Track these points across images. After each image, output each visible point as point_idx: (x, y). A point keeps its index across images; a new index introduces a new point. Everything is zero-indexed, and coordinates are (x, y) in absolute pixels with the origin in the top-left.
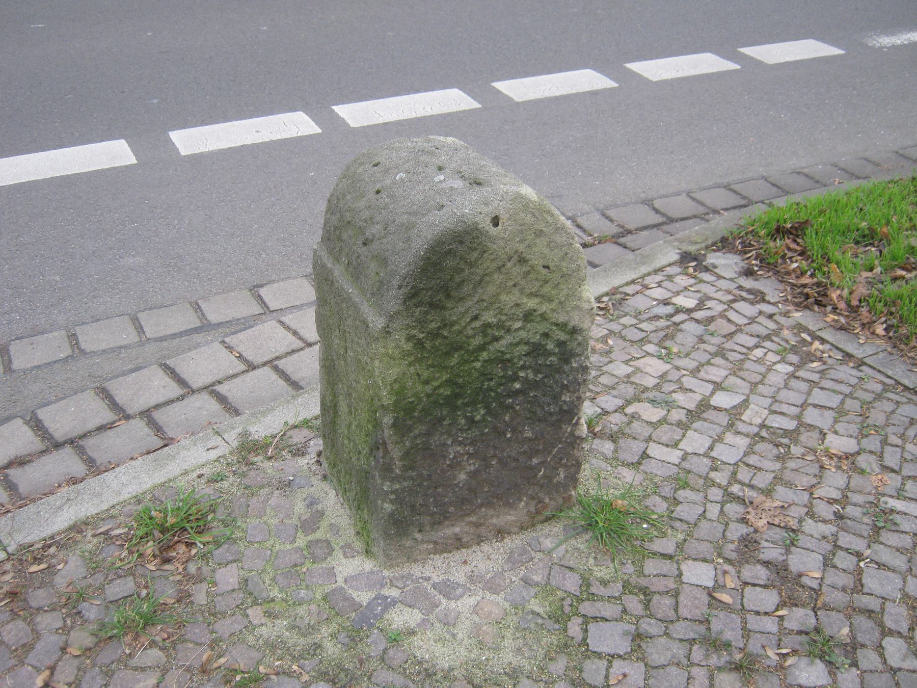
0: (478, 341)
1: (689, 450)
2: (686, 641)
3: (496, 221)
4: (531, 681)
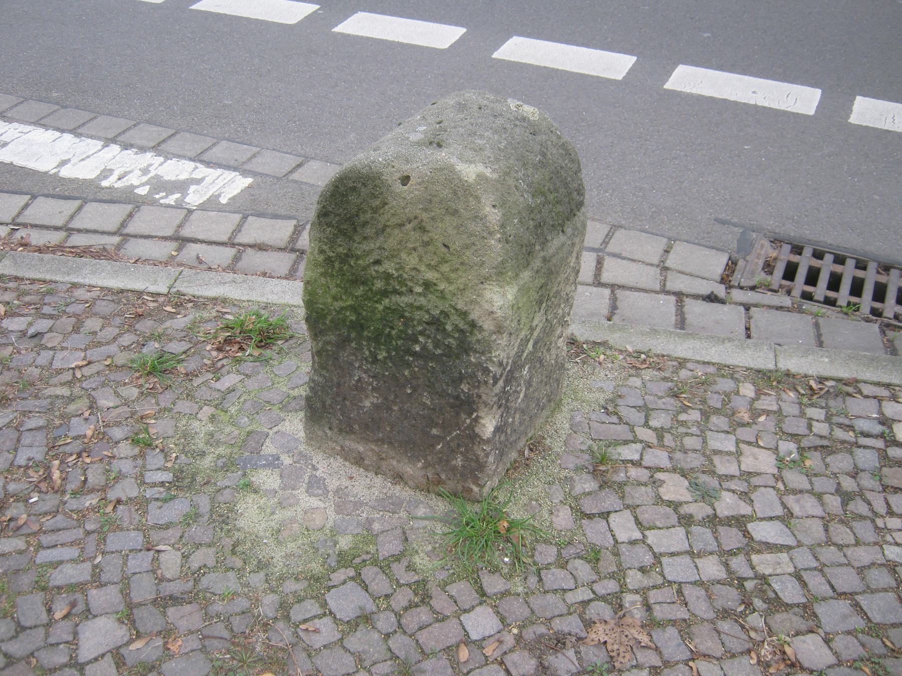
0: (379, 285)
1: (649, 541)
2: (392, 652)
3: (405, 180)
4: (265, 578)
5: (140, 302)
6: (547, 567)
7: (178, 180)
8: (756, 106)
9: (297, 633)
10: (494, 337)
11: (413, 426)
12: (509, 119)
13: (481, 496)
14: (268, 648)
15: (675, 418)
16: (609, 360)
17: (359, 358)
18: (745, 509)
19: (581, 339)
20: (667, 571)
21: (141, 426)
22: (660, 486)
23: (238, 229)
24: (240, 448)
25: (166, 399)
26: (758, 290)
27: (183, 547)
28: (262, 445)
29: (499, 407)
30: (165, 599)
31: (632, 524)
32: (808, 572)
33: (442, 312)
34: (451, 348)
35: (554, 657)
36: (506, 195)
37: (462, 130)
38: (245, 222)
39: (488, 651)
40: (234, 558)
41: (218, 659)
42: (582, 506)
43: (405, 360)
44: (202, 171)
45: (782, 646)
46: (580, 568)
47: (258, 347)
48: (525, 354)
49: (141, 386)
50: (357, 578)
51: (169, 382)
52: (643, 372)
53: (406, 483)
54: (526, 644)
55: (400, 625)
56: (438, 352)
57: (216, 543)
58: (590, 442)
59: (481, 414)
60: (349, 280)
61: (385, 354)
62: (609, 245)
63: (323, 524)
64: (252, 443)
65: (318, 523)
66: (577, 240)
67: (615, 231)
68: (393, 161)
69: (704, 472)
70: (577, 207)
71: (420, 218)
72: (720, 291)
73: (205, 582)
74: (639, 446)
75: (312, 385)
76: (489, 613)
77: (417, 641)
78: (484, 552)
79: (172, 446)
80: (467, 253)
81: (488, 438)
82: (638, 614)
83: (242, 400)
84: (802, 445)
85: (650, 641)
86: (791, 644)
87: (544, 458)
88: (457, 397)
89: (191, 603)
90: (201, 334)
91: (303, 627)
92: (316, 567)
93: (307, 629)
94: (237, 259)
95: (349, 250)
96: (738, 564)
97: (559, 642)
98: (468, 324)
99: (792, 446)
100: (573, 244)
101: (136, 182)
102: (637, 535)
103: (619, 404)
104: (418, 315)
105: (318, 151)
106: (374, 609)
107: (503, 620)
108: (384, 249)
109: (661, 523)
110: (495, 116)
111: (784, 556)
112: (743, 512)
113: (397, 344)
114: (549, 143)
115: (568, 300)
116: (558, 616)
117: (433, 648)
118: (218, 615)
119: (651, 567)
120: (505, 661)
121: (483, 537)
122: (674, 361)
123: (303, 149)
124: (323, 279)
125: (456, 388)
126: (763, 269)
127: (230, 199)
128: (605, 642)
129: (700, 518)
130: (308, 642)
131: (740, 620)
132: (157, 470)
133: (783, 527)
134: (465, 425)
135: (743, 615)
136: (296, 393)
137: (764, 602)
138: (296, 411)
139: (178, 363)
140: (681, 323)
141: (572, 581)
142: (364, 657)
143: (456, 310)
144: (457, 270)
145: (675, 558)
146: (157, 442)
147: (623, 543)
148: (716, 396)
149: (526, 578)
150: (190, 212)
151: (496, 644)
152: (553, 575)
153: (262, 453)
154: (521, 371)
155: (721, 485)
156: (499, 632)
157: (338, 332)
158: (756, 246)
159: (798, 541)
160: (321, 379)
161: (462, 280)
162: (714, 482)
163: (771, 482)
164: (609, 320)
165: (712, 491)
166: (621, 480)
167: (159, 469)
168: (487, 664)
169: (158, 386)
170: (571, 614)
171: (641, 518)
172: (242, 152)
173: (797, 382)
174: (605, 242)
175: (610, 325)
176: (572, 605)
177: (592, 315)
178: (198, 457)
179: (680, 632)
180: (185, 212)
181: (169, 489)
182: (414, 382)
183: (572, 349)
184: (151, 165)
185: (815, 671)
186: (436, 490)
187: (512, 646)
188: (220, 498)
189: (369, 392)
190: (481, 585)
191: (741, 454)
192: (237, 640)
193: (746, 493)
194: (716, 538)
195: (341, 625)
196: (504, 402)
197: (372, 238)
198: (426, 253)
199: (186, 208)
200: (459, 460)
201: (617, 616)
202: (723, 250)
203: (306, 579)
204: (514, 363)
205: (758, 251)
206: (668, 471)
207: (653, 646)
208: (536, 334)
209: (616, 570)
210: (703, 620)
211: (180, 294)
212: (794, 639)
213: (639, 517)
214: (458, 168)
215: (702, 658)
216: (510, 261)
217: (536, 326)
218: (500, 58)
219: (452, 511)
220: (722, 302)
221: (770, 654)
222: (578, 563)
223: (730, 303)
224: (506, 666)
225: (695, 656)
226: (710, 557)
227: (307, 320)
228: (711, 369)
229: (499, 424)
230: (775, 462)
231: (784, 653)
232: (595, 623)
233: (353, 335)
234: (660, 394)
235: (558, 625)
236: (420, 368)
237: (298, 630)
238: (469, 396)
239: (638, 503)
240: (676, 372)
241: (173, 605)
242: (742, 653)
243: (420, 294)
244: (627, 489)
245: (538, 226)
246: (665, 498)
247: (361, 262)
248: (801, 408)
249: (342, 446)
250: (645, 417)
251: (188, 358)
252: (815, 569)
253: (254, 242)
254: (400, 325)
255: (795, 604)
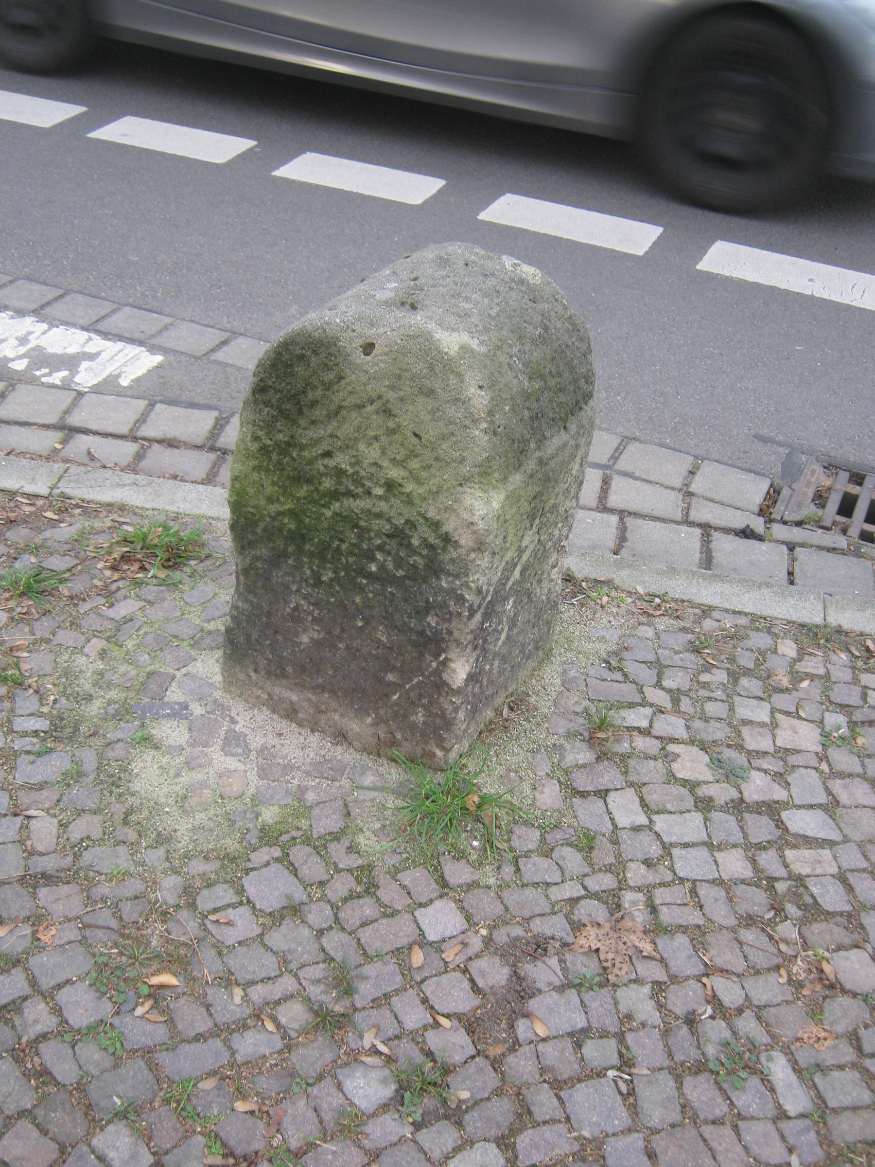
0: (328, 484)
1: (657, 828)
3: (369, 348)
4: (165, 855)
5: (12, 504)
6: (527, 854)
7: (67, 354)
8: (812, 298)
9: (204, 925)
10: (473, 555)
11: (363, 669)
12: (503, 280)
13: (446, 763)
14: (167, 942)
15: (695, 678)
16: (615, 603)
17: (298, 579)
18: (779, 794)
19: (579, 575)
20: (678, 866)
21: (11, 660)
22: (673, 761)
23: (143, 419)
24: (138, 692)
25: (43, 627)
26: (805, 526)
27: (61, 813)
28: (167, 690)
29: (475, 649)
30: (35, 877)
31: (636, 805)
32: (856, 873)
33: (408, 522)
34: (417, 568)
35: (532, 965)
36: (496, 374)
37: (443, 290)
38: (151, 410)
39: (449, 956)
40: (126, 829)
41: (102, 954)
42: (574, 781)
43: (356, 583)
44: (97, 343)
45: (820, 962)
46: (568, 857)
47: (164, 567)
48: (510, 583)
49: (11, 610)
50: (285, 860)
51: (48, 606)
52: (657, 619)
53: (350, 744)
54: (497, 948)
55: (337, 920)
56: (401, 573)
57: (103, 810)
58: (586, 703)
59: (452, 656)
60: (289, 477)
61: (331, 575)
62: (619, 461)
63: (242, 790)
64: (153, 687)
65: (236, 789)
66: (582, 441)
67: (627, 444)
68: (353, 324)
69: (729, 746)
70: (584, 398)
71: (385, 399)
72: (758, 524)
73: (87, 858)
74: (648, 711)
75: (235, 613)
76: (451, 909)
77: (359, 940)
78: (447, 833)
79: (50, 686)
80: (444, 446)
81: (459, 687)
82: (640, 917)
83: (141, 632)
84: (854, 718)
85: (654, 950)
86: (830, 961)
87: (527, 720)
88: (422, 633)
89: (68, 883)
90: (91, 548)
91: (212, 917)
92: (232, 845)
93: (218, 921)
94: (139, 456)
95: (292, 437)
96: (768, 860)
97: (539, 947)
98: (440, 537)
99: (841, 719)
100: (577, 446)
101: (11, 354)
102: (642, 820)
103: (625, 658)
104: (376, 524)
105: (249, 326)
106: (305, 898)
107: (468, 917)
108: (336, 436)
109: (673, 806)
110: (486, 275)
111: (826, 854)
112: (776, 797)
113: (348, 562)
114: (553, 314)
115: (567, 518)
116: (539, 915)
117: (379, 950)
118: (104, 900)
119: (658, 860)
120: (469, 968)
121: (447, 815)
122: (696, 608)
123: (229, 322)
124: (255, 474)
125: (420, 621)
126: (813, 500)
127: (133, 381)
128: (597, 950)
129: (723, 803)
130: (218, 937)
131: (768, 929)
132: (29, 715)
133: (826, 817)
134: (430, 669)
135: (772, 923)
136: (211, 626)
137: (799, 908)
138: (212, 649)
139: (61, 583)
140: (707, 562)
141: (559, 873)
142: (290, 958)
143: (426, 519)
144: (430, 466)
145: (689, 849)
146: (30, 681)
147: (625, 828)
148: (747, 654)
149: (499, 868)
150: (80, 394)
151: (460, 947)
152: (534, 864)
153: (166, 699)
154: (504, 605)
155: (750, 763)
156: (463, 933)
157: (271, 545)
158: (805, 471)
159: (845, 836)
160: (246, 606)
161: (436, 480)
162: (741, 759)
163: (814, 762)
164: (615, 553)
165: (738, 770)
166: (624, 751)
167: (32, 715)
168: (447, 972)
169: (33, 610)
170: (555, 913)
171: (648, 798)
172: (150, 323)
173: (850, 641)
174: (615, 458)
175: (617, 560)
176: (557, 903)
177: (593, 547)
178: (83, 702)
179: (692, 940)
180: (74, 394)
181: (44, 740)
182: (367, 612)
183: (567, 588)
184: (31, 333)
185: (859, 994)
186: (389, 753)
187: (479, 950)
188: (111, 754)
189: (308, 624)
190: (442, 873)
191: (777, 726)
192: (127, 931)
193: (781, 774)
194: (742, 828)
195: (262, 917)
196: (480, 641)
197: (322, 423)
198: (391, 443)
199: (75, 390)
200: (420, 714)
201: (613, 918)
202: (763, 475)
203: (217, 858)
204: (496, 592)
205: (808, 478)
206: (684, 743)
207: (658, 956)
208: (525, 558)
209: (614, 861)
210: (721, 927)
211: (64, 496)
212: (834, 954)
213: (645, 797)
214: (437, 336)
215: (720, 973)
216: (498, 458)
217: (526, 547)
218: (487, 220)
219: (408, 780)
220: (760, 538)
221: (804, 971)
222: (567, 851)
223: (770, 541)
224: (470, 975)
225: (709, 970)
226: (734, 851)
227: (233, 527)
228: (743, 621)
229: (473, 670)
230: (819, 737)
231: (822, 971)
232: (585, 925)
233: (291, 549)
234: (677, 648)
235: (539, 926)
236: (375, 594)
237: (206, 921)
238: (437, 632)
239: (645, 781)
240: (698, 621)
241: (45, 886)
242: (769, 970)
243: (380, 497)
244: (632, 763)
245: (535, 418)
246: (680, 775)
247: (306, 454)
248: (854, 673)
249: (269, 694)
250: (657, 676)
251: (74, 577)
252: (864, 870)
253: (163, 437)
254: (352, 536)
255: (837, 913)
